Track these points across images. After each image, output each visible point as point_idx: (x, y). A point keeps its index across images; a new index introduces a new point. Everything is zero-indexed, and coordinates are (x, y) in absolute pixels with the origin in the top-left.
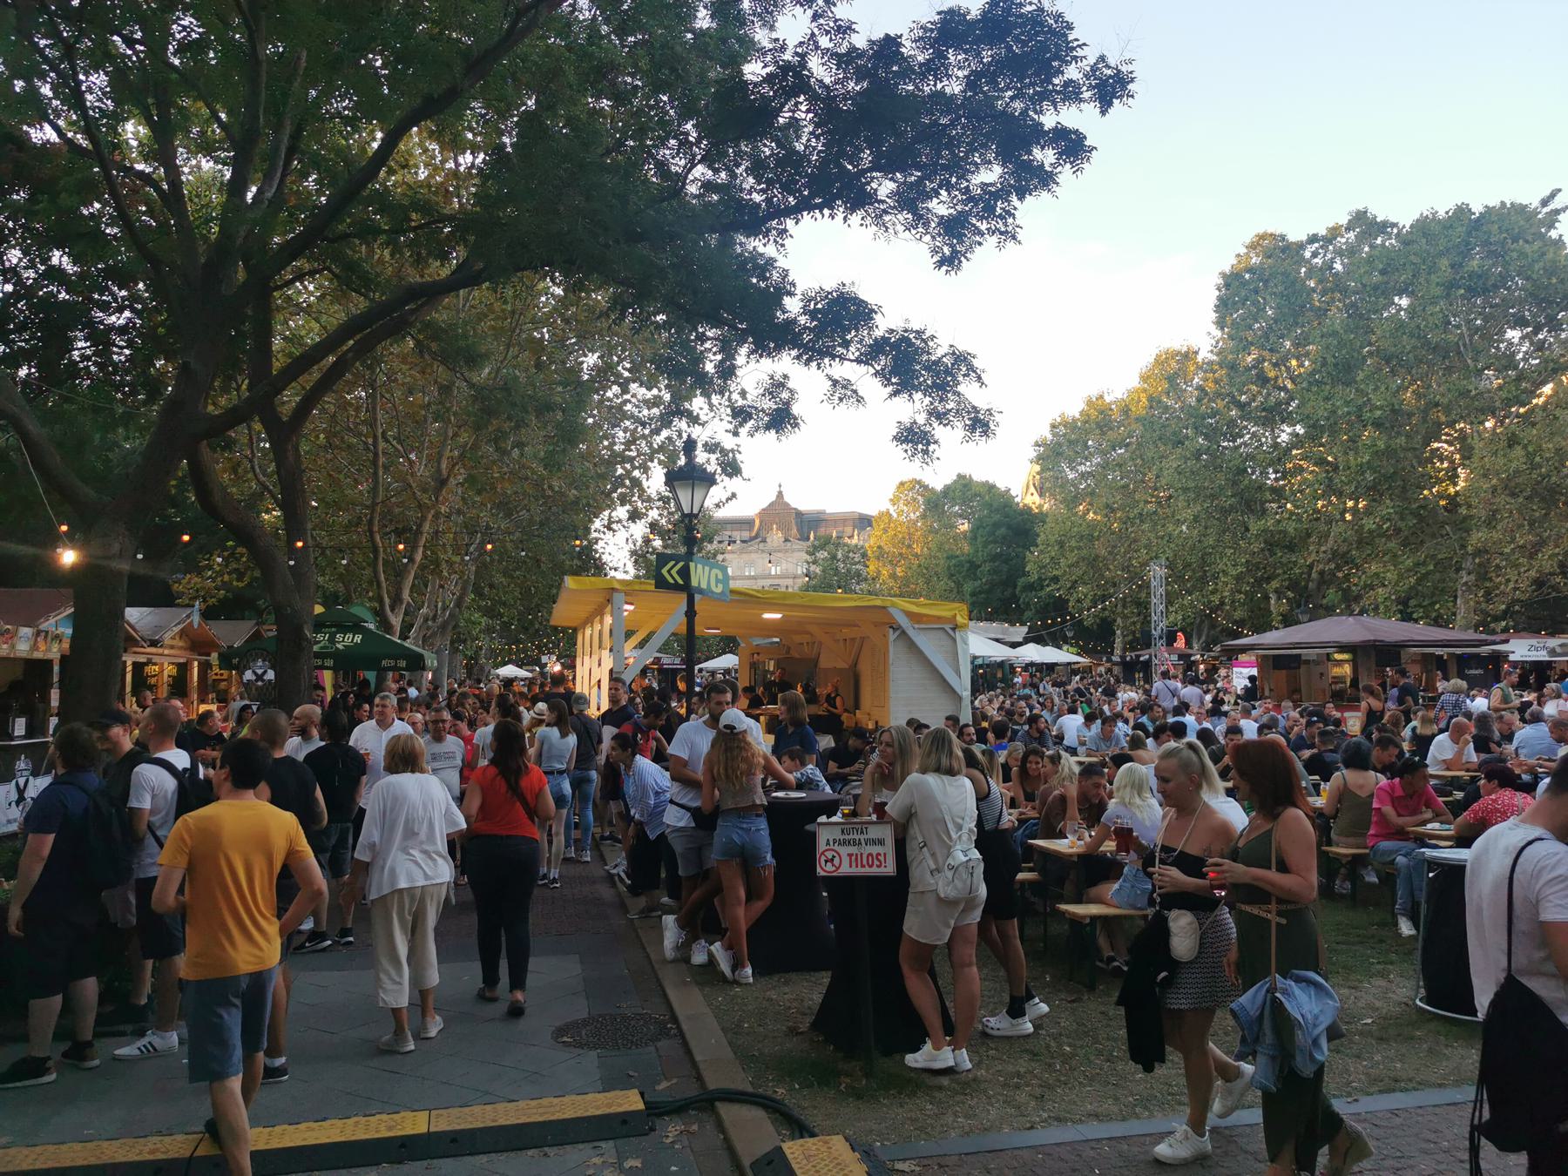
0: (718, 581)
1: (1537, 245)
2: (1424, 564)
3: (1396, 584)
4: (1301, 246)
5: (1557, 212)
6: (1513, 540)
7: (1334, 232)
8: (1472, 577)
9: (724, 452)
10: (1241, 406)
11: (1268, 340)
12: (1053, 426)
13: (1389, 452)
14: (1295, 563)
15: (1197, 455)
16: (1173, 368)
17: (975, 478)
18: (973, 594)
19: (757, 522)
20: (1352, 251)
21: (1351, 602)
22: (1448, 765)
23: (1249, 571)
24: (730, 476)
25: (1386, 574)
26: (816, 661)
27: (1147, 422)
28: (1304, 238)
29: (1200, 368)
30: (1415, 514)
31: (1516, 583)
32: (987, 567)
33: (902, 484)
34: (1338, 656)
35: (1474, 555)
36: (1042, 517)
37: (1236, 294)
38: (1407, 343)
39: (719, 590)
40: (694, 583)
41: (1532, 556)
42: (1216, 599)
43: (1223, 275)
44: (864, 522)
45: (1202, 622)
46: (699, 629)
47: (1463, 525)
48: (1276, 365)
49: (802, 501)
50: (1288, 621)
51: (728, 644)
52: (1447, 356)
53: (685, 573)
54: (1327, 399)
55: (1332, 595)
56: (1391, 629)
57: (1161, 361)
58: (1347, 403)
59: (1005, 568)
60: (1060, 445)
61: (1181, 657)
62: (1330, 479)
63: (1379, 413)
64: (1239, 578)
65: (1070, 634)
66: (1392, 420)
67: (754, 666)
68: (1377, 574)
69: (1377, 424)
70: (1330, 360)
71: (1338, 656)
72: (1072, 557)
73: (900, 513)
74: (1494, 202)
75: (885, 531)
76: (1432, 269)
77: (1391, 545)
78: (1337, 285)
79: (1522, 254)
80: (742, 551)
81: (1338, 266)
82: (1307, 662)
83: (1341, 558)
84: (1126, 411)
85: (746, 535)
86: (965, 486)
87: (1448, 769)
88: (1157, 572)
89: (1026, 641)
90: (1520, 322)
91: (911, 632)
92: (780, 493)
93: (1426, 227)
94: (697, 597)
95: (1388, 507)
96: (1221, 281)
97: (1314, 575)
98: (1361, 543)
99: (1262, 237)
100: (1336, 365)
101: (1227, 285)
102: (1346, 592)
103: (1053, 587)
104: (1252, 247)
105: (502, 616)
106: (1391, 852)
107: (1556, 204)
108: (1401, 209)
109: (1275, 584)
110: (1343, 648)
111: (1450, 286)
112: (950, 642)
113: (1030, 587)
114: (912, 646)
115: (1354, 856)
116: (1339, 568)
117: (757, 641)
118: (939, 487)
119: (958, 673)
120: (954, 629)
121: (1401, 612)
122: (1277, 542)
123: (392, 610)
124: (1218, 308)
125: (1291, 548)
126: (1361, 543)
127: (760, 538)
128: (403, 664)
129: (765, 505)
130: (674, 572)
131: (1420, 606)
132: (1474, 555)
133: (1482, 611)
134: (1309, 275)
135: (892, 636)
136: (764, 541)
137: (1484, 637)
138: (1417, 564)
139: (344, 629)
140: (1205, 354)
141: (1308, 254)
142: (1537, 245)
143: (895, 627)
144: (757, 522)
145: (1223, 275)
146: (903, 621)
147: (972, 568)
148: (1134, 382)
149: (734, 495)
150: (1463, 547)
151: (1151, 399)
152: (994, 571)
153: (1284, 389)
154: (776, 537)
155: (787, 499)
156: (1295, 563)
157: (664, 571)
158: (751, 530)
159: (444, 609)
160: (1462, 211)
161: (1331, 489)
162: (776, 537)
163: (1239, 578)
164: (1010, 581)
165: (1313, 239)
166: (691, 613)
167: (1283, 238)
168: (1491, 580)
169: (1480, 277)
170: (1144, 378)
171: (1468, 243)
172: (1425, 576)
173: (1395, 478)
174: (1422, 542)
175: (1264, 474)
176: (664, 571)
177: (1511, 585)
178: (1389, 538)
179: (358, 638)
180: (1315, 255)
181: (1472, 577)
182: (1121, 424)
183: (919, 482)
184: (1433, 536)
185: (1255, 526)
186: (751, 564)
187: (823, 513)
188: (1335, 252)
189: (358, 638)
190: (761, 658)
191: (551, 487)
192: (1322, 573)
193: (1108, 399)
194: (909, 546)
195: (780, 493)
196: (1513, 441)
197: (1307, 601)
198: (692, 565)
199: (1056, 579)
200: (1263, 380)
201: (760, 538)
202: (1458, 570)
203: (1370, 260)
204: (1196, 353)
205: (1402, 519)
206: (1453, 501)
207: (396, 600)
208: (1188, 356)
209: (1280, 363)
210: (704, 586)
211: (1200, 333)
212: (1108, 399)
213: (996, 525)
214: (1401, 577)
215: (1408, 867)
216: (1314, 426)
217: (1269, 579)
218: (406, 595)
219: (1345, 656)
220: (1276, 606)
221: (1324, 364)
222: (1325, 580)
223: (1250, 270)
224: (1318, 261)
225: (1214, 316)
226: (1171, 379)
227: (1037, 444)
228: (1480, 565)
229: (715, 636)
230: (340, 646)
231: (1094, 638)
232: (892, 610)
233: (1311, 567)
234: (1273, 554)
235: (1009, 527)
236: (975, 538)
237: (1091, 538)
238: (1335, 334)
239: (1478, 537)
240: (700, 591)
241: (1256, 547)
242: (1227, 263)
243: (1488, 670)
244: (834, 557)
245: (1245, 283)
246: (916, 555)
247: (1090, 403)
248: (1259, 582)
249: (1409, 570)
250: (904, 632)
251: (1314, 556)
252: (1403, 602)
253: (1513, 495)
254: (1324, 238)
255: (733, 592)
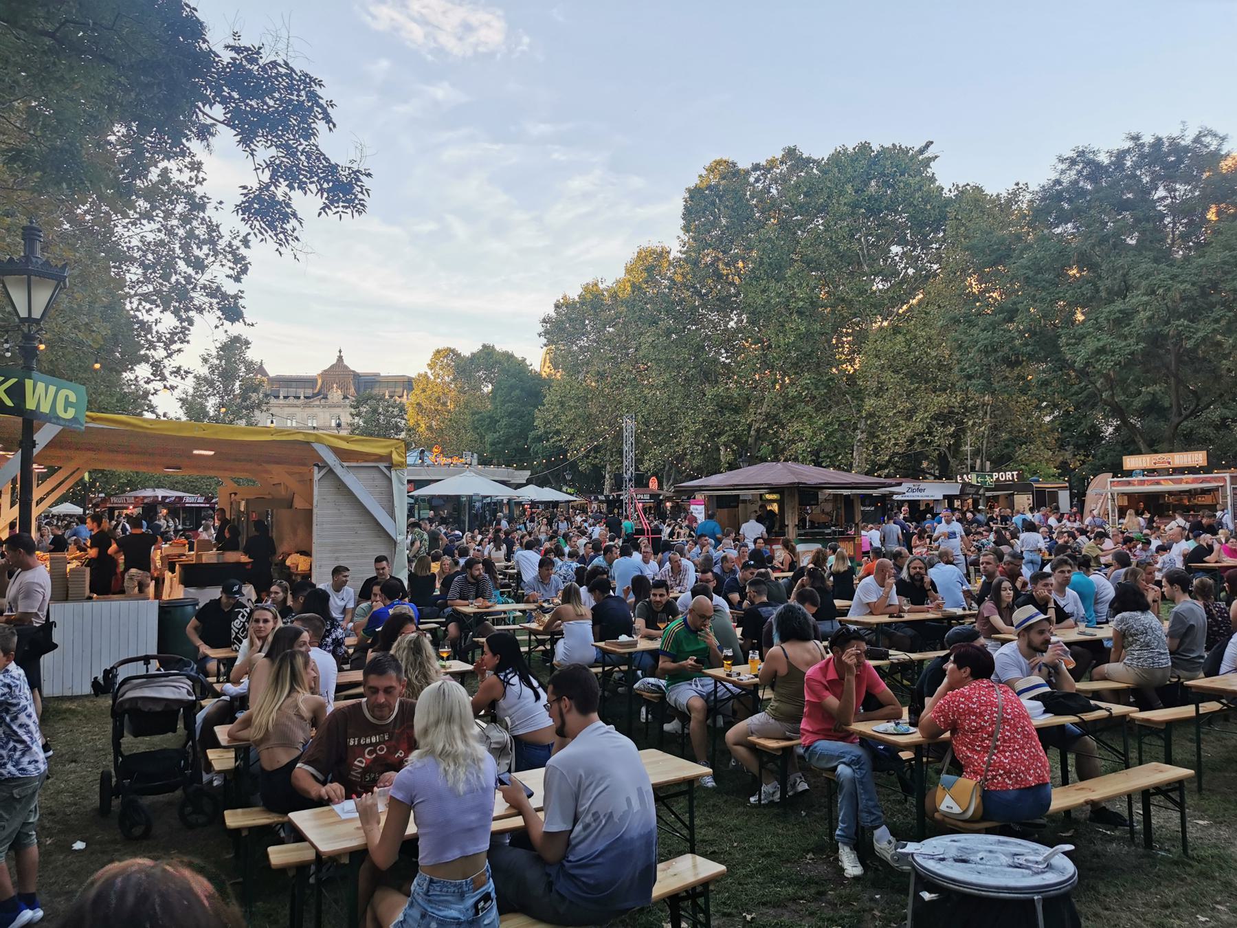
1: (918, 178)
2: (831, 424)
3: (811, 439)
4: (747, 173)
5: (930, 160)
6: (895, 407)
7: (772, 164)
8: (865, 435)
9: (225, 296)
10: (701, 296)
11: (722, 245)
12: (557, 306)
13: (808, 336)
14: (739, 422)
15: (668, 333)
16: (650, 263)
17: (498, 348)
18: (492, 444)
19: (320, 382)
20: (784, 179)
21: (777, 454)
22: (872, 609)
23: (705, 427)
24: (233, 321)
25: (804, 430)
27: (630, 304)
28: (749, 166)
29: (670, 264)
30: (827, 386)
31: (895, 439)
32: (504, 422)
33: (438, 352)
34: (768, 497)
35: (867, 418)
36: (548, 382)
37: (699, 205)
38: (823, 251)
40: (30, 405)
41: (909, 418)
42: (679, 450)
43: (689, 190)
44: (408, 384)
45: (670, 468)
47: (859, 395)
48: (727, 264)
49: (359, 364)
50: (732, 467)
52: (851, 262)
54: (763, 291)
55: (765, 448)
56: (811, 474)
57: (643, 255)
58: (779, 295)
59: (519, 423)
60: (562, 322)
61: (652, 496)
62: (765, 355)
63: (801, 303)
64: (697, 434)
65: (568, 478)
66: (810, 310)
68: (797, 432)
69: (800, 313)
70: (766, 260)
71: (768, 497)
72: (571, 415)
73: (437, 376)
74: (888, 145)
75: (424, 391)
76: (842, 193)
77: (809, 408)
78: (769, 207)
79: (907, 184)
80: (305, 406)
81: (774, 191)
82: (744, 501)
83: (771, 418)
84: (614, 296)
85: (309, 392)
86: (488, 354)
87: (871, 613)
88: (629, 425)
89: (529, 482)
90: (902, 242)
91: (339, 471)
92: (340, 357)
93: (837, 159)
95: (807, 378)
96: (687, 195)
97: (752, 433)
98: (786, 407)
99: (719, 163)
100: (770, 264)
101: (691, 197)
102: (775, 445)
103: (556, 438)
104: (711, 170)
106: (832, 758)
107: (929, 153)
108: (819, 149)
109: (723, 439)
110: (773, 489)
111: (855, 206)
112: (385, 483)
113: (539, 439)
114: (342, 488)
115: (784, 749)
116: (770, 426)
118: (468, 354)
119: (392, 515)
120: (389, 468)
121: (813, 461)
122: (725, 406)
124: (685, 217)
125: (736, 410)
126: (786, 407)
127: (322, 395)
131: (828, 457)
132: (867, 418)
133: (873, 461)
134: (752, 197)
135: (317, 475)
136: (325, 398)
137: (882, 480)
138: (827, 424)
140: (676, 251)
141: (752, 180)
142: (918, 178)
143: (321, 465)
144: (320, 382)
145: (689, 190)
146: (331, 459)
147: (493, 422)
148: (621, 274)
150: (859, 411)
151: (633, 285)
152: (511, 426)
153: (732, 284)
154: (336, 395)
155: (346, 362)
156: (739, 422)
158: (314, 387)
160: (864, 148)
161: (767, 365)
162: (336, 395)
163: (697, 434)
164: (523, 434)
165: (756, 167)
167: (734, 165)
168: (878, 437)
169: (876, 200)
170: (629, 271)
171: (868, 174)
172: (831, 434)
173: (811, 358)
174: (830, 407)
175: (718, 353)
177: (893, 441)
178: (807, 403)
180: (757, 180)
181: (865, 435)
182: (610, 308)
183: (453, 351)
184: (837, 404)
185: (710, 392)
186: (314, 417)
187: (377, 375)
188: (772, 179)
192: (758, 430)
193: (601, 286)
194: (444, 404)
195: (340, 357)
196: (896, 330)
197: (746, 454)
198: (29, 383)
199: (558, 433)
200: (719, 276)
201: (322, 395)
202: (855, 429)
203: (797, 186)
204: (669, 253)
205: (817, 388)
206: (852, 379)
208: (662, 254)
209: (731, 263)
211: (671, 237)
212: (601, 286)
213: (512, 388)
214: (815, 433)
215: (853, 781)
216: (753, 313)
217: (719, 435)
219: (775, 497)
220: (725, 456)
221: (761, 264)
222: (761, 436)
223: (709, 187)
224: (760, 185)
225: (682, 222)
226: (649, 270)
227: (544, 321)
228: (870, 426)
231: (589, 482)
232: (316, 446)
233: (750, 426)
234: (723, 414)
235: (522, 389)
236: (494, 398)
237: (586, 400)
238: (769, 240)
239: (870, 403)
241: (710, 409)
242: (693, 182)
243: (883, 509)
244: (375, 411)
245: (705, 197)
246: (449, 412)
247: (586, 288)
248: (712, 436)
249: (820, 429)
250: (331, 471)
251: (753, 418)
252: (816, 454)
253: (897, 372)
254: (764, 168)
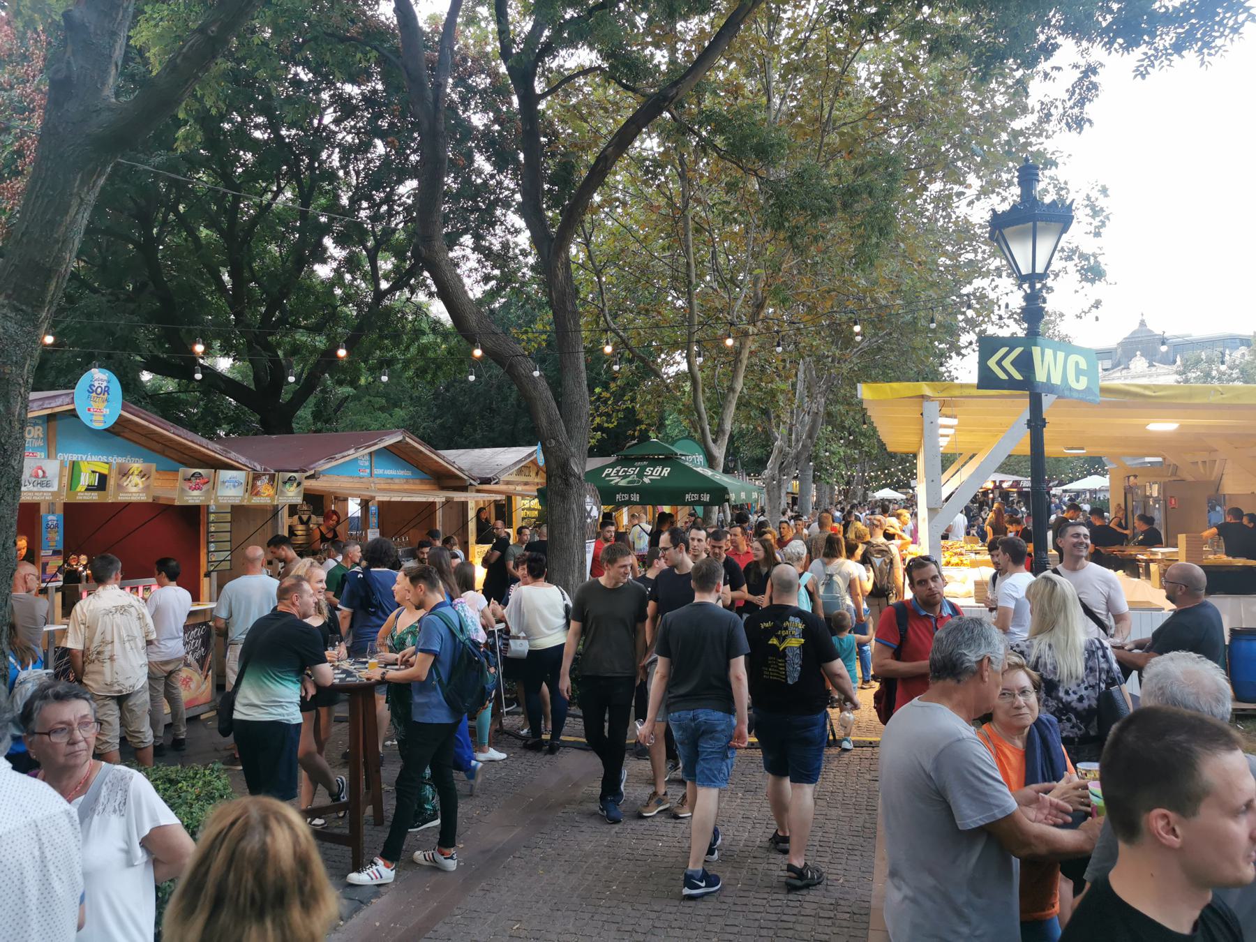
0: (1079, 372)
9: (1083, 257)
24: (1092, 281)
26: (1218, 485)
39: (1082, 384)
40: (1040, 376)
46: (1050, 449)
51: (1094, 465)
53: (1025, 363)
67: (1128, 491)
94: (1047, 401)
105: (862, 445)
117: (1130, 462)
123: (715, 441)
128: (706, 498)
129: (1127, 335)
130: (1007, 363)
139: (654, 462)
144: (1119, 351)
149: (1097, 304)
155: (1150, 327)
157: (992, 363)
159: (797, 441)
166: (1036, 424)
176: (992, 363)
179: (666, 471)
189: (666, 471)
190: (1139, 481)
191: (874, 300)
198: (1036, 351)
207: (718, 433)
210: (1056, 380)
218: (728, 426)
229: (1078, 457)
230: (646, 480)
240: (1051, 388)
255: (1105, 391)
